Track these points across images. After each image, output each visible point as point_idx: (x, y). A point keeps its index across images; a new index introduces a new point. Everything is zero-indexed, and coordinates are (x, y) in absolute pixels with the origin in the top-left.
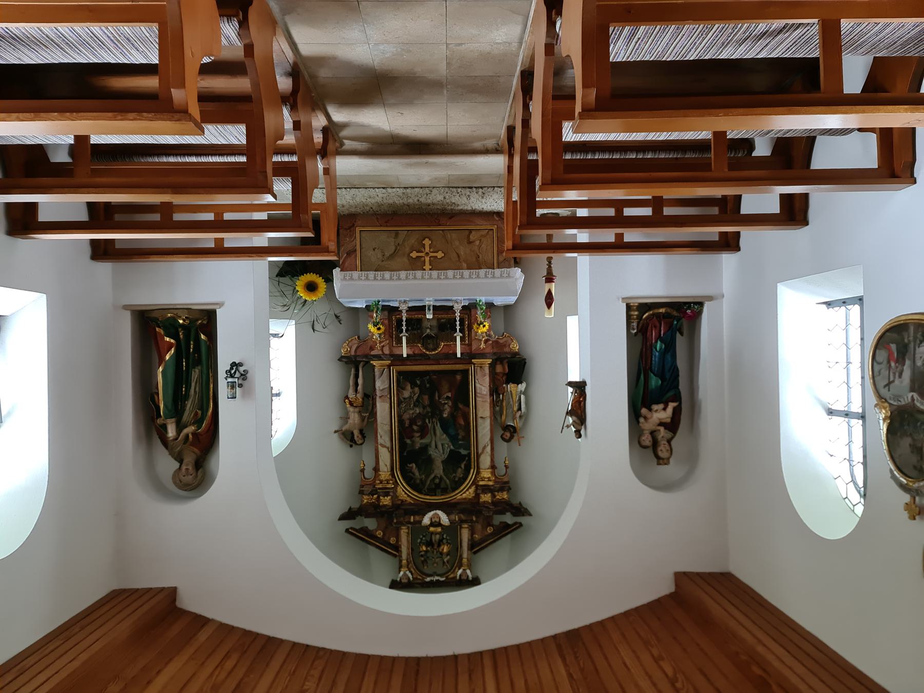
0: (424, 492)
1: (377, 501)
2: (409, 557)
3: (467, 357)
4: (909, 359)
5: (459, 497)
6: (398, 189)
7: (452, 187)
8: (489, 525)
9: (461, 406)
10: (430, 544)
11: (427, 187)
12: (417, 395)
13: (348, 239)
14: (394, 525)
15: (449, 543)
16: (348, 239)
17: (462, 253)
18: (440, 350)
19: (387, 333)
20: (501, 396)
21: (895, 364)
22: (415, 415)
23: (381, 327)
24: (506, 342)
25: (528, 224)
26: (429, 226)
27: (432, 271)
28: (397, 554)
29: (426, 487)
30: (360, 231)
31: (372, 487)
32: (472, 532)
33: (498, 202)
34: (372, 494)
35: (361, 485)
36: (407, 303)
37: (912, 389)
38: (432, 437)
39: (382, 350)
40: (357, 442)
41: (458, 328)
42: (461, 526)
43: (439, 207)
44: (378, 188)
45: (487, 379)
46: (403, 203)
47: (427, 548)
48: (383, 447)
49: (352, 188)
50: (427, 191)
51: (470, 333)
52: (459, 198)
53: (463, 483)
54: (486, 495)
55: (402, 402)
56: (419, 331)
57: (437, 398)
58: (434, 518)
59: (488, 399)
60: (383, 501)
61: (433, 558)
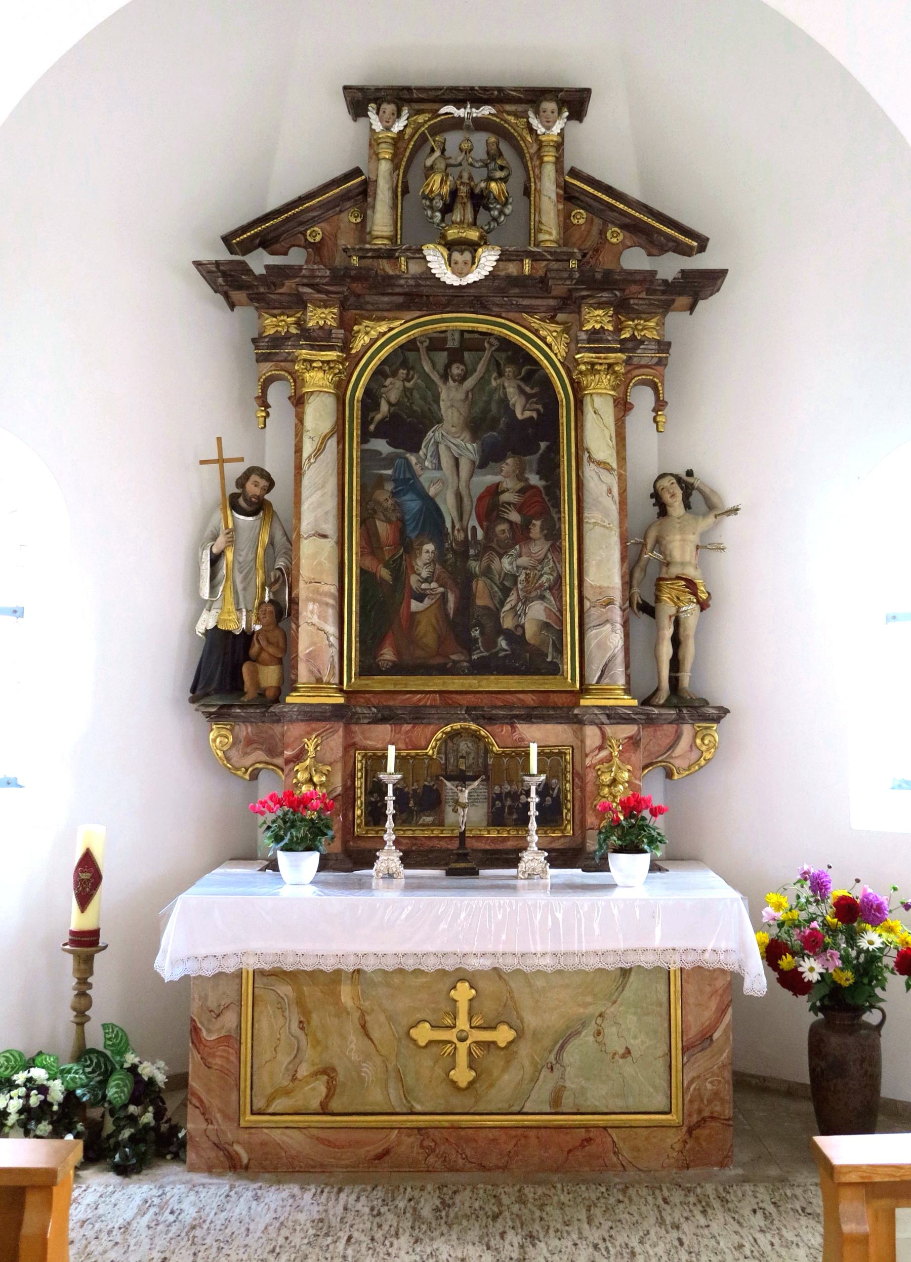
0: (492, 340)
8: (317, 248)
9: (385, 573)
10: (480, 200)
12: (507, 607)
15: (425, 197)
16: (709, 1086)
17: (352, 1037)
18: (439, 735)
20: (267, 599)
22: (513, 552)
24: (246, 754)
26: (455, 1128)
28: (567, 178)
29: (487, 354)
31: (635, 361)
32: (362, 228)
34: (633, 344)
35: (666, 365)
38: (468, 486)
40: (674, 481)
41: (390, 798)
45: (304, 646)
48: (605, 463)
51: (349, 783)
53: (384, 362)
54: (321, 323)
55: (550, 588)
56: (497, 789)
57: (451, 598)
59: (303, 591)
61: (471, 165)
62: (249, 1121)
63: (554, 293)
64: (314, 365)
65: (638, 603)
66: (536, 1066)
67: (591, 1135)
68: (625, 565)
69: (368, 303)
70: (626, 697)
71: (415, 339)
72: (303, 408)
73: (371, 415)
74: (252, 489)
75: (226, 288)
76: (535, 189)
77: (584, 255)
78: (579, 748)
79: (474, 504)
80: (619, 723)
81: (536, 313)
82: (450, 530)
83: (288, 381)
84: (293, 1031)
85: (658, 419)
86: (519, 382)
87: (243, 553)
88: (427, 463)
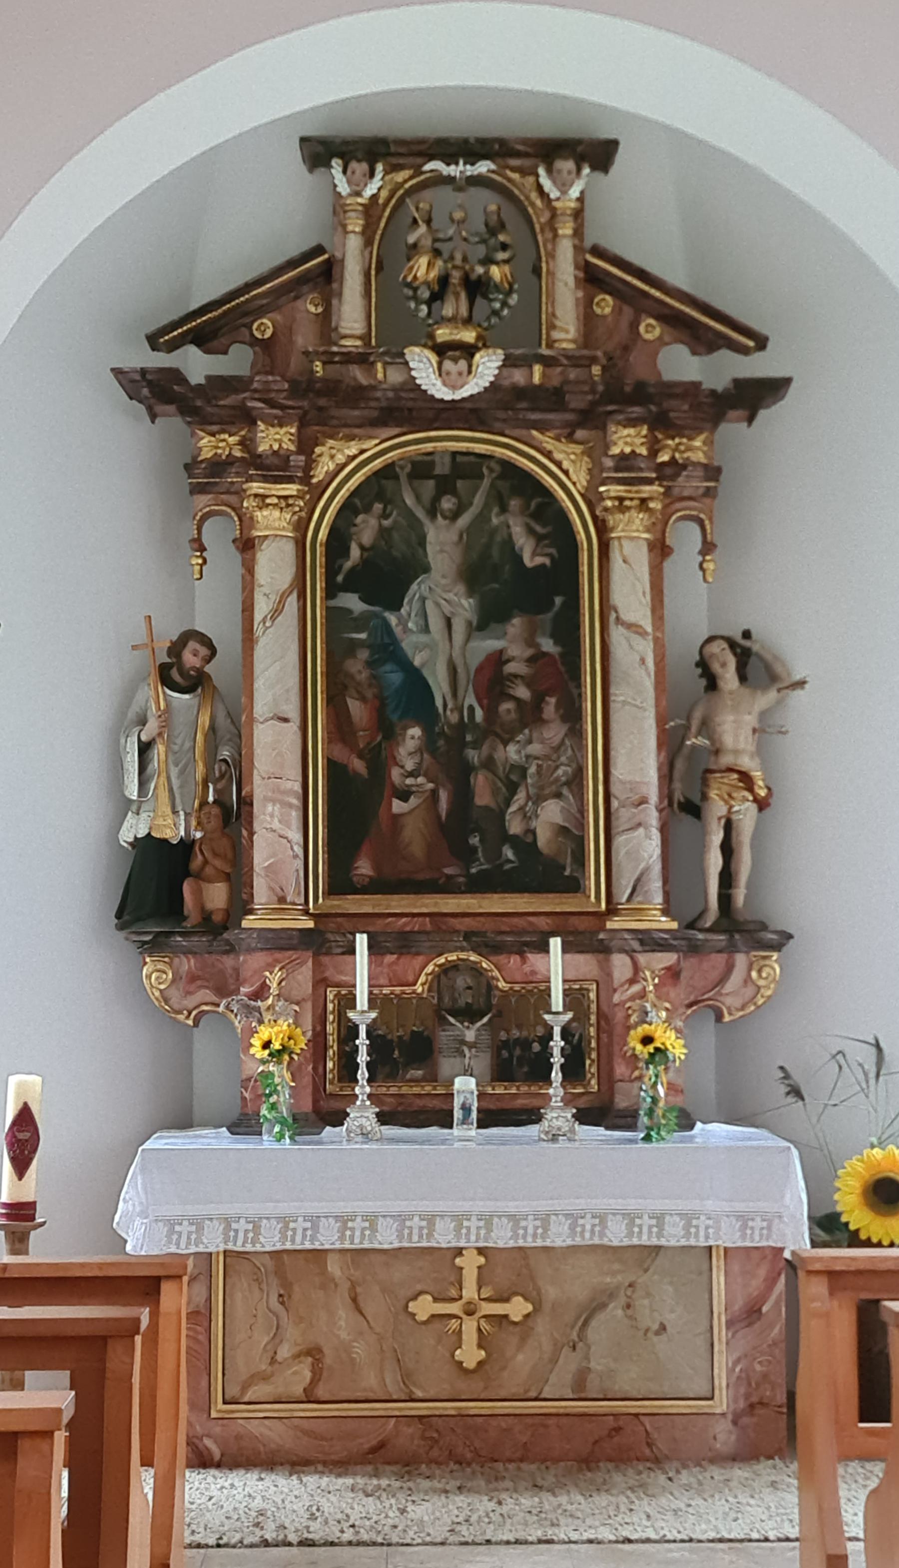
1: (657, 441)
2: (549, 246)
3: (330, 937)
5: (372, 446)
6: (574, 1536)
7: (374, 1544)
8: (266, 346)
9: (358, 765)
11: (466, 1543)
12: (513, 808)
13: (758, 1368)
14: (599, 353)
15: (409, 285)
16: (758, 1368)
17: (342, 1313)
18: (430, 968)
19: (619, 1030)
20: (211, 799)
22: (520, 737)
23: (639, 1047)
24: (188, 993)
25: (104, 1340)
27: (453, 1244)
28: (589, 257)
29: (486, 482)
30: (712, 1398)
31: (676, 492)
33: (204, 1499)
34: (675, 468)
35: (714, 497)
36: (547, 1133)
39: (636, 968)
40: (725, 645)
41: (362, 1041)
42: (367, 344)
43: (426, 1484)
44: (648, 1541)
45: (261, 858)
46: (554, 1495)
47: (487, 272)
49: (741, 1541)
50: (466, 1533)
51: (319, 1028)
52: (349, 1511)
53: (354, 494)
54: (276, 447)
56: (503, 1036)
58: (460, 374)
59: (259, 788)
60: (639, 441)
62: (219, 1411)
63: (573, 405)
64: (268, 501)
65: (679, 803)
66: (555, 1345)
67: (621, 1423)
68: (663, 754)
69: (333, 417)
70: (663, 919)
71: (393, 463)
72: (254, 555)
73: (339, 562)
74: (191, 658)
75: (152, 401)
76: (548, 270)
77: (610, 359)
78: (605, 983)
79: (472, 677)
80: (653, 951)
81: (548, 430)
82: (441, 710)
83: (232, 518)
84: (271, 1306)
85: (705, 565)
86: (529, 520)
87: (179, 741)
88: (410, 625)
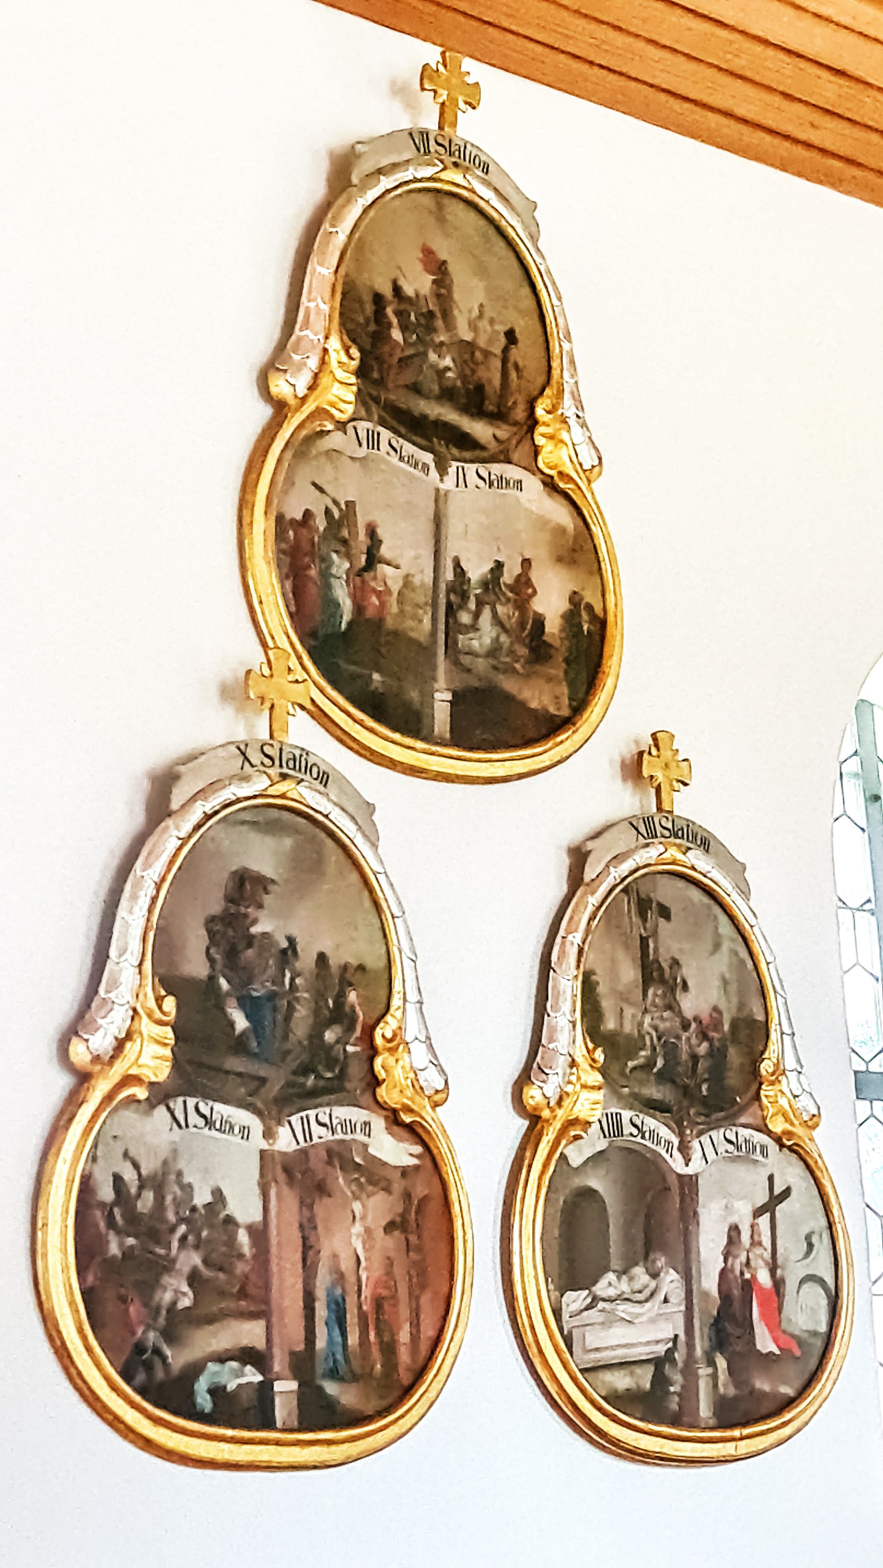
4: (706, 1295)
21: (754, 1277)
37: (689, 1184)
